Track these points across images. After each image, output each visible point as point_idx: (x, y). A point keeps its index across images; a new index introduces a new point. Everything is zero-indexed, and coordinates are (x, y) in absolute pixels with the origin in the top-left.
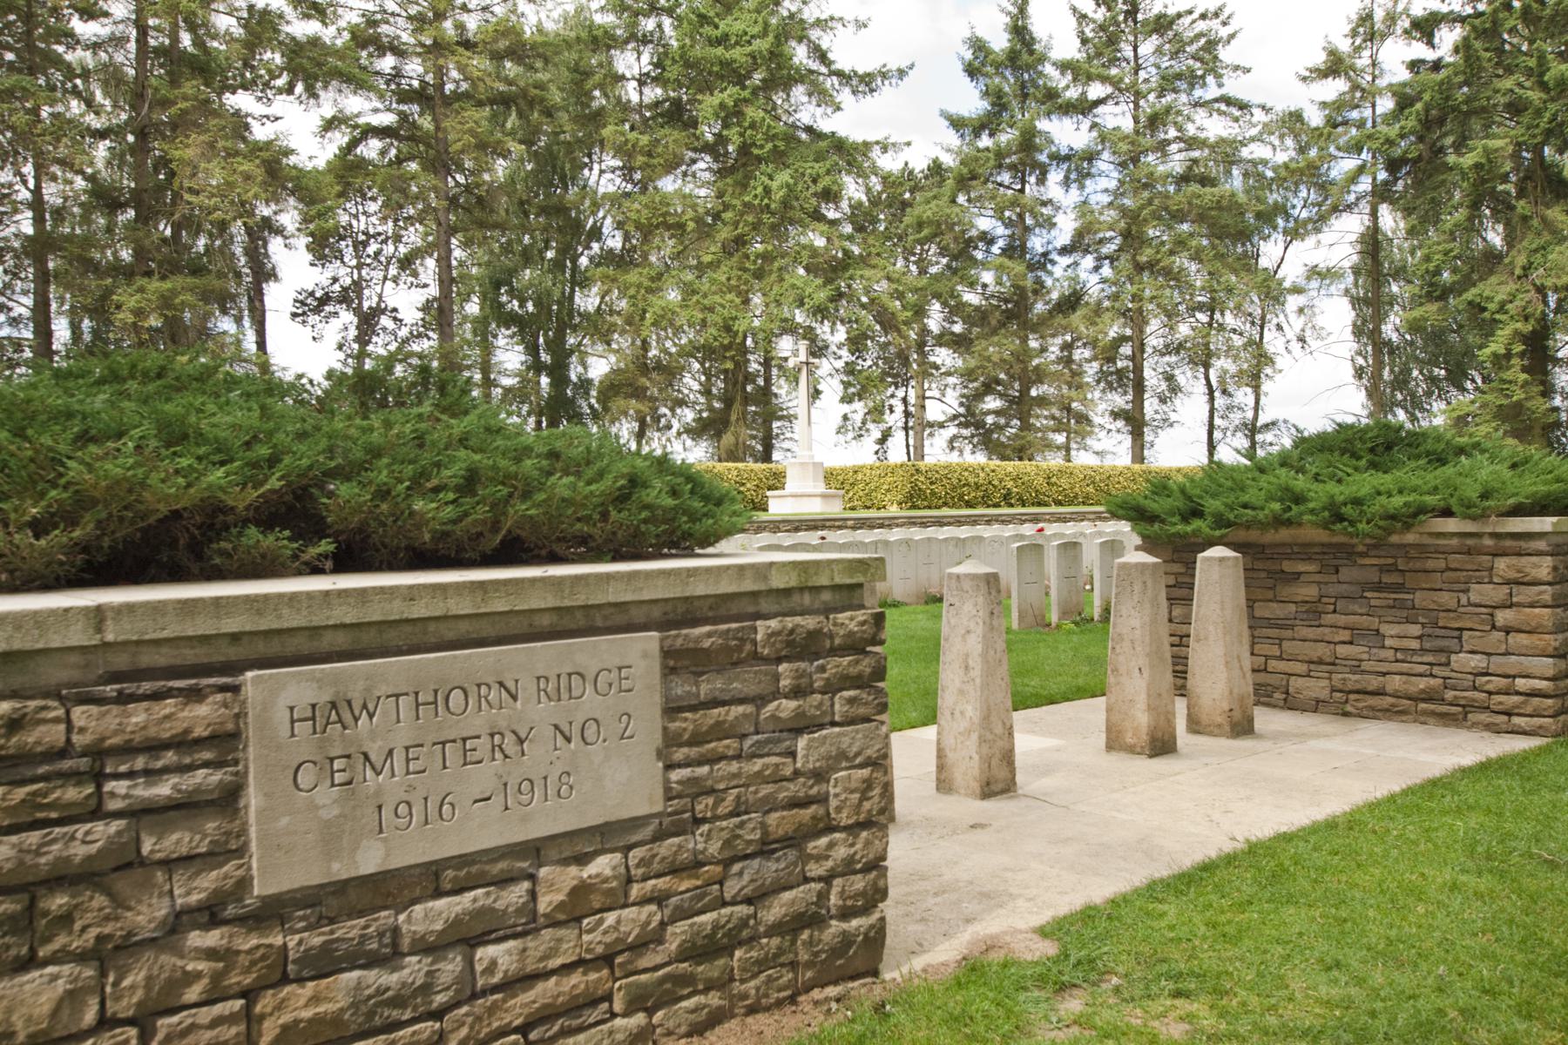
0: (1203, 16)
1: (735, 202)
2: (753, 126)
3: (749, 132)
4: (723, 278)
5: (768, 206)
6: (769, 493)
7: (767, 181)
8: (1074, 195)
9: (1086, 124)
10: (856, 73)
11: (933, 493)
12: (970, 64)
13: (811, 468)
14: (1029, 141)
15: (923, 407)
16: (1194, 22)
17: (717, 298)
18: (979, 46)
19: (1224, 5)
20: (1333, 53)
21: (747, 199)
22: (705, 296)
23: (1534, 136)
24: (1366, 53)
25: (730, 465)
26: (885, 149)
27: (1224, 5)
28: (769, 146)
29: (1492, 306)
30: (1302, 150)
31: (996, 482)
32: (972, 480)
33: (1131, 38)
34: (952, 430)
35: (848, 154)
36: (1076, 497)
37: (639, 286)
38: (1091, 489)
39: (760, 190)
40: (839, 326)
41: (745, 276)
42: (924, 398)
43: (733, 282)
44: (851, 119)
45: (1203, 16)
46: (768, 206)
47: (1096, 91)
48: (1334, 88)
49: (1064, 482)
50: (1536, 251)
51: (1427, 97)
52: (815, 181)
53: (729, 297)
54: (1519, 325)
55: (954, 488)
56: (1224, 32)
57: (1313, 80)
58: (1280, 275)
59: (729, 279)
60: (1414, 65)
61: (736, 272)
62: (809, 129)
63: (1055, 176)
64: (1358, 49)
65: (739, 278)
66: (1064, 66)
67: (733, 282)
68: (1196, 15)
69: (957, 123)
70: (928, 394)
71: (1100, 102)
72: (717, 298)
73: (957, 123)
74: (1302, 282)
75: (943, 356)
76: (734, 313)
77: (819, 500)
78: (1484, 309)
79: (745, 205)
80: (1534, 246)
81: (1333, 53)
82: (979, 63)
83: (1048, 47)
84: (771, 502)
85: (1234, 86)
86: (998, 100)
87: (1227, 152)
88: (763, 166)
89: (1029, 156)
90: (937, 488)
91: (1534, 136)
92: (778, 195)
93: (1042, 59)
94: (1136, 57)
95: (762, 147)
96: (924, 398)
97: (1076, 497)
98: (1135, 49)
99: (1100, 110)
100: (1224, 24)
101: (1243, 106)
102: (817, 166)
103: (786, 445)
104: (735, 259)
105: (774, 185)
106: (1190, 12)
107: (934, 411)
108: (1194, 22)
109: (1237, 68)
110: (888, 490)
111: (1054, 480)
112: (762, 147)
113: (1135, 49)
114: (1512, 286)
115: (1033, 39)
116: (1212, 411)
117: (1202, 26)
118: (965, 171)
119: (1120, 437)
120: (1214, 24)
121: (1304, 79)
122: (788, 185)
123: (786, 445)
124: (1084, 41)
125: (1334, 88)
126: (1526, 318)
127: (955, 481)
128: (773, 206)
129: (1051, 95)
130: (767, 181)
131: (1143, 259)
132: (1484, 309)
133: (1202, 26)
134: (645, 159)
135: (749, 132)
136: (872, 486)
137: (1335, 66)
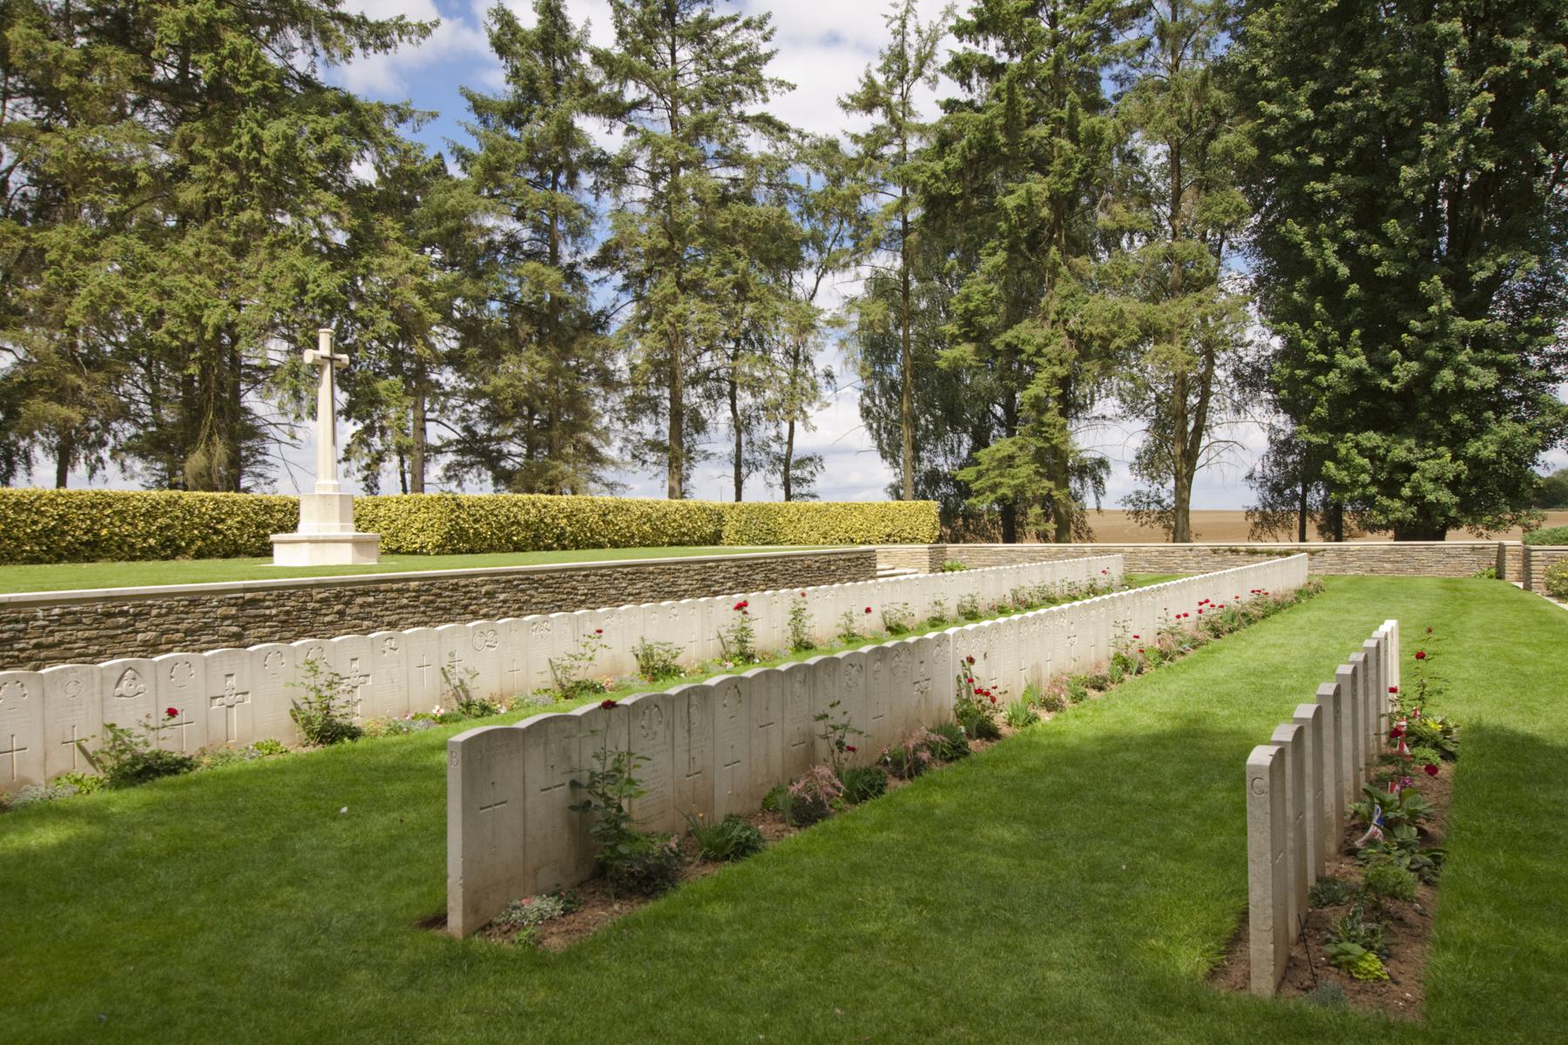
0: (747, 25)
1: (207, 152)
2: (234, 55)
3: (228, 62)
4: (190, 252)
5: (257, 161)
6: (273, 537)
7: (256, 129)
8: (607, 203)
9: (620, 127)
10: (365, 21)
11: (477, 533)
12: (498, 37)
13: (337, 502)
14: (567, 135)
15: (424, 430)
16: (737, 29)
17: (181, 280)
18: (506, 20)
19: (769, 15)
20: (871, 85)
21: (227, 149)
22: (163, 274)
23: (1066, 185)
24: (898, 91)
25: (202, 494)
26: (401, 118)
27: (769, 15)
28: (257, 85)
29: (1030, 349)
30: (837, 181)
31: (548, 520)
32: (521, 518)
33: (669, 39)
34: (450, 457)
35: (360, 122)
36: (633, 536)
37: (65, 249)
38: (647, 528)
39: (246, 139)
40: (860, 148)
41: (222, 251)
42: (425, 420)
43: (204, 259)
44: (363, 75)
45: (747, 25)
46: (257, 161)
47: (632, 92)
48: (864, 123)
49: (621, 521)
50: (1066, 297)
51: (969, 135)
52: (319, 140)
53: (197, 278)
54: (1056, 369)
55: (501, 528)
56: (764, 48)
57: (853, 109)
58: (816, 303)
59: (198, 254)
60: (950, 106)
61: (206, 247)
62: (305, 81)
63: (586, 179)
64: (891, 86)
65: (213, 253)
66: (601, 58)
67: (204, 259)
68: (739, 24)
69: (480, 107)
70: (429, 415)
71: (636, 105)
72: (181, 280)
73: (480, 107)
74: (842, 313)
75: (447, 377)
76: (203, 300)
77: (349, 546)
78: (1022, 351)
79: (222, 157)
80: (1064, 293)
81: (871, 85)
82: (506, 38)
83: (585, 33)
84: (277, 548)
85: (778, 107)
86: (531, 91)
87: (774, 168)
88: (250, 110)
89: (560, 158)
90: (482, 528)
91: (1066, 185)
92: (273, 149)
93: (577, 47)
94: (674, 61)
95: (247, 84)
96: (425, 420)
97: (633, 536)
98: (673, 53)
99: (633, 114)
100: (766, 39)
101: (782, 129)
102: (322, 120)
103: (257, 469)
104: (206, 228)
105: (266, 135)
106: (735, 20)
107: (435, 433)
108: (737, 29)
109: (781, 84)
110: (422, 530)
111: (610, 517)
112: (247, 84)
113: (673, 53)
114: (1048, 331)
115: (566, 24)
116: (739, 445)
117: (744, 36)
118: (493, 159)
119: (655, 469)
120: (752, 36)
121: (845, 106)
122: (286, 137)
123: (257, 469)
124: (622, 35)
125: (864, 123)
126: (1061, 363)
127: (503, 519)
128: (264, 162)
129: (587, 88)
130: (256, 129)
131: (686, 276)
132: (1022, 351)
133: (744, 36)
134: (74, 80)
135: (228, 62)
136: (400, 523)
137: (869, 100)
